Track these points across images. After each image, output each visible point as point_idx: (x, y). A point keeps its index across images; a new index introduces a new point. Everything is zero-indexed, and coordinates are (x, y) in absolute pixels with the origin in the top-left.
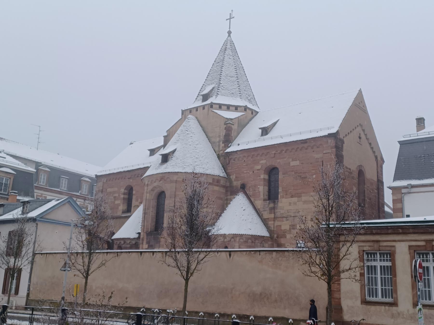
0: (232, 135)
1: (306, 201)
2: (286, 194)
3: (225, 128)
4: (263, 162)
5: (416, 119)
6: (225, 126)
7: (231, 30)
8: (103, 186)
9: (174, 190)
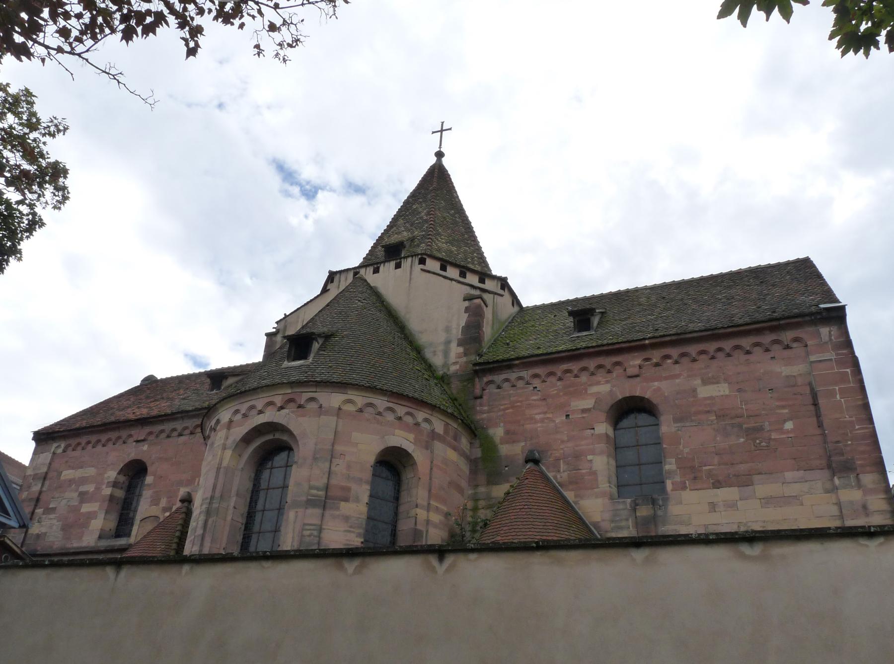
1: (771, 497)
3: (467, 310)
8: (50, 464)
9: (332, 436)
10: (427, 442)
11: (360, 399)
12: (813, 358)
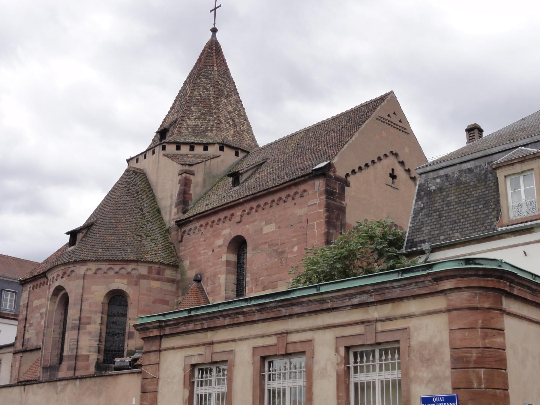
0: (191, 192)
2: (257, 285)
4: (226, 232)
5: (466, 130)
6: (180, 177)
7: (216, 26)
8: (29, 297)
9: (81, 291)
10: (136, 281)
11: (93, 267)
12: (310, 203)
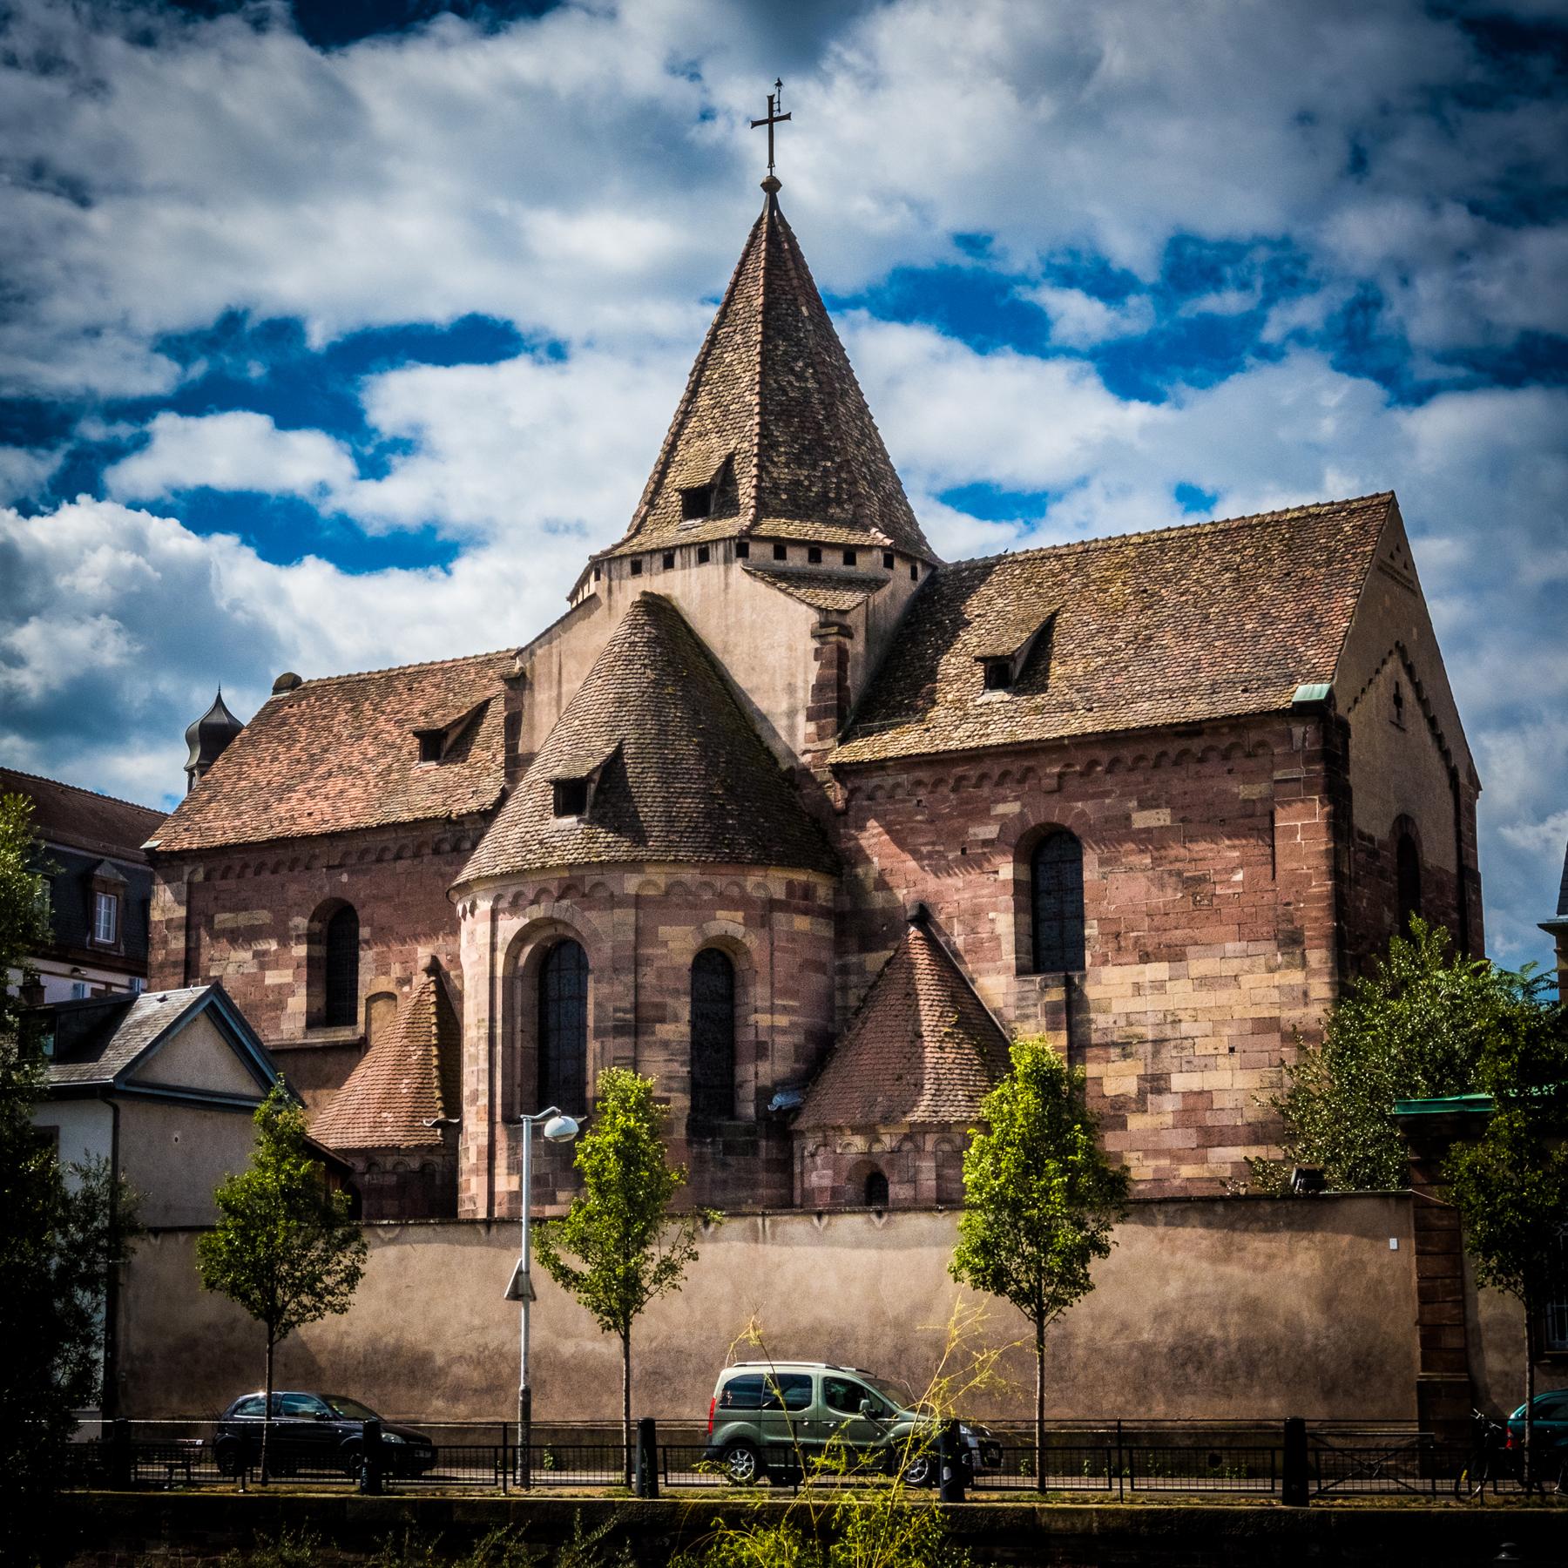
1: (1206, 977)
4: (1011, 808)
7: (777, 174)
9: (632, 937)
12: (1278, 775)
